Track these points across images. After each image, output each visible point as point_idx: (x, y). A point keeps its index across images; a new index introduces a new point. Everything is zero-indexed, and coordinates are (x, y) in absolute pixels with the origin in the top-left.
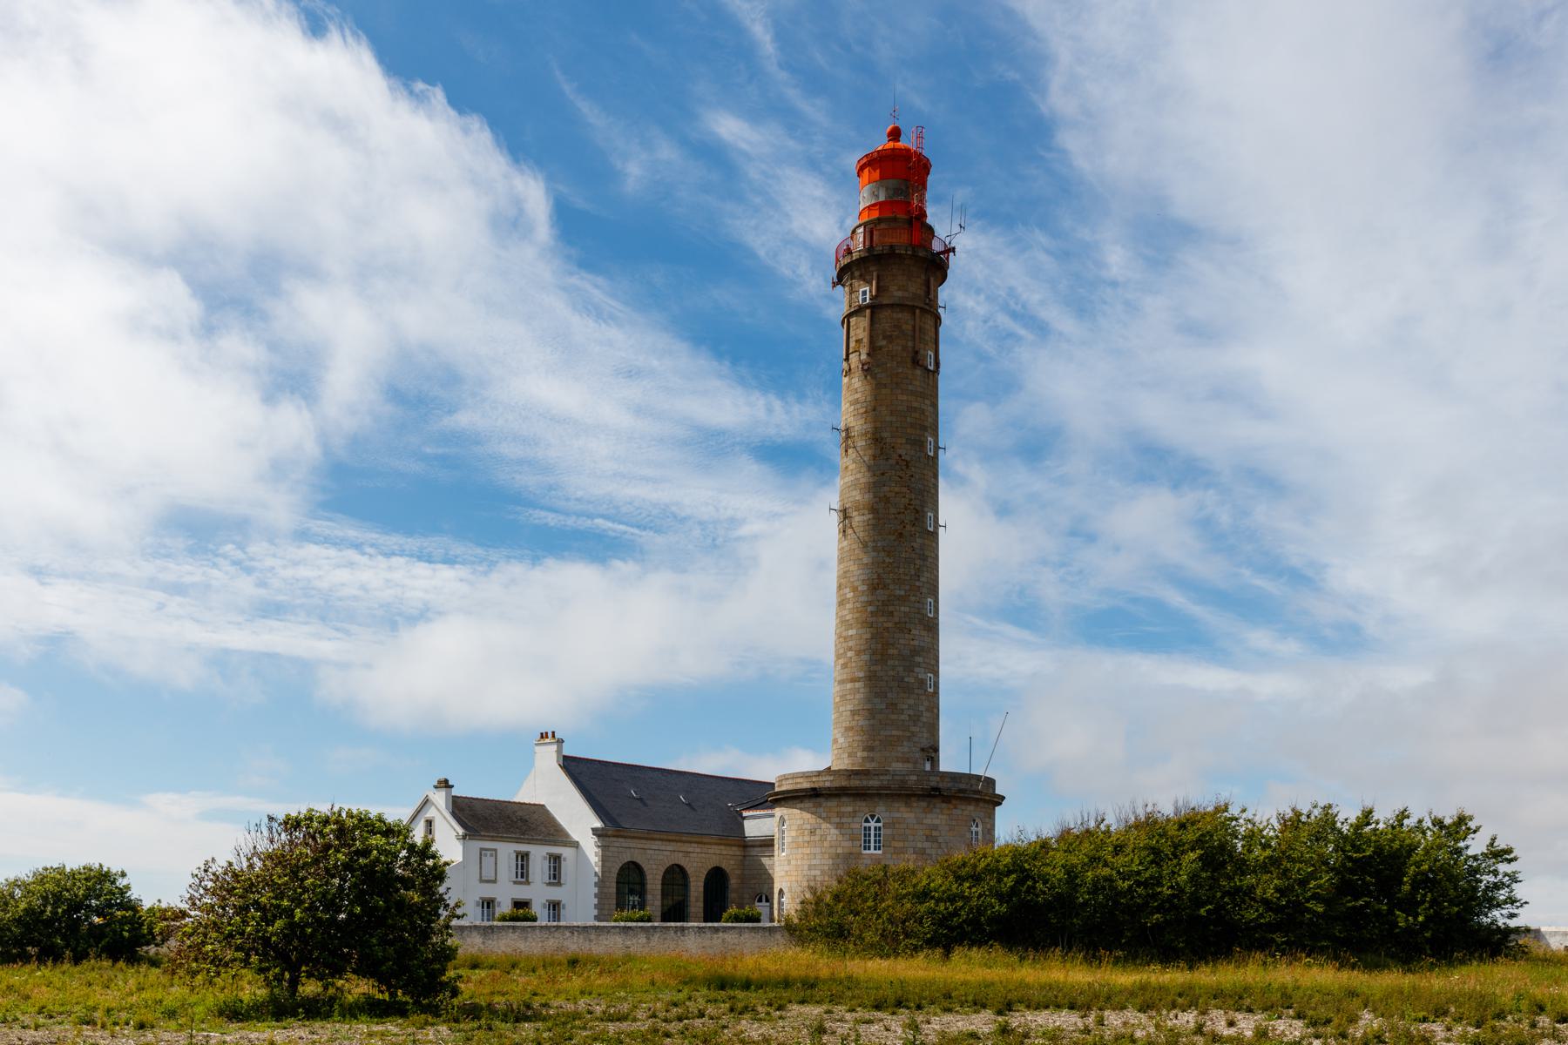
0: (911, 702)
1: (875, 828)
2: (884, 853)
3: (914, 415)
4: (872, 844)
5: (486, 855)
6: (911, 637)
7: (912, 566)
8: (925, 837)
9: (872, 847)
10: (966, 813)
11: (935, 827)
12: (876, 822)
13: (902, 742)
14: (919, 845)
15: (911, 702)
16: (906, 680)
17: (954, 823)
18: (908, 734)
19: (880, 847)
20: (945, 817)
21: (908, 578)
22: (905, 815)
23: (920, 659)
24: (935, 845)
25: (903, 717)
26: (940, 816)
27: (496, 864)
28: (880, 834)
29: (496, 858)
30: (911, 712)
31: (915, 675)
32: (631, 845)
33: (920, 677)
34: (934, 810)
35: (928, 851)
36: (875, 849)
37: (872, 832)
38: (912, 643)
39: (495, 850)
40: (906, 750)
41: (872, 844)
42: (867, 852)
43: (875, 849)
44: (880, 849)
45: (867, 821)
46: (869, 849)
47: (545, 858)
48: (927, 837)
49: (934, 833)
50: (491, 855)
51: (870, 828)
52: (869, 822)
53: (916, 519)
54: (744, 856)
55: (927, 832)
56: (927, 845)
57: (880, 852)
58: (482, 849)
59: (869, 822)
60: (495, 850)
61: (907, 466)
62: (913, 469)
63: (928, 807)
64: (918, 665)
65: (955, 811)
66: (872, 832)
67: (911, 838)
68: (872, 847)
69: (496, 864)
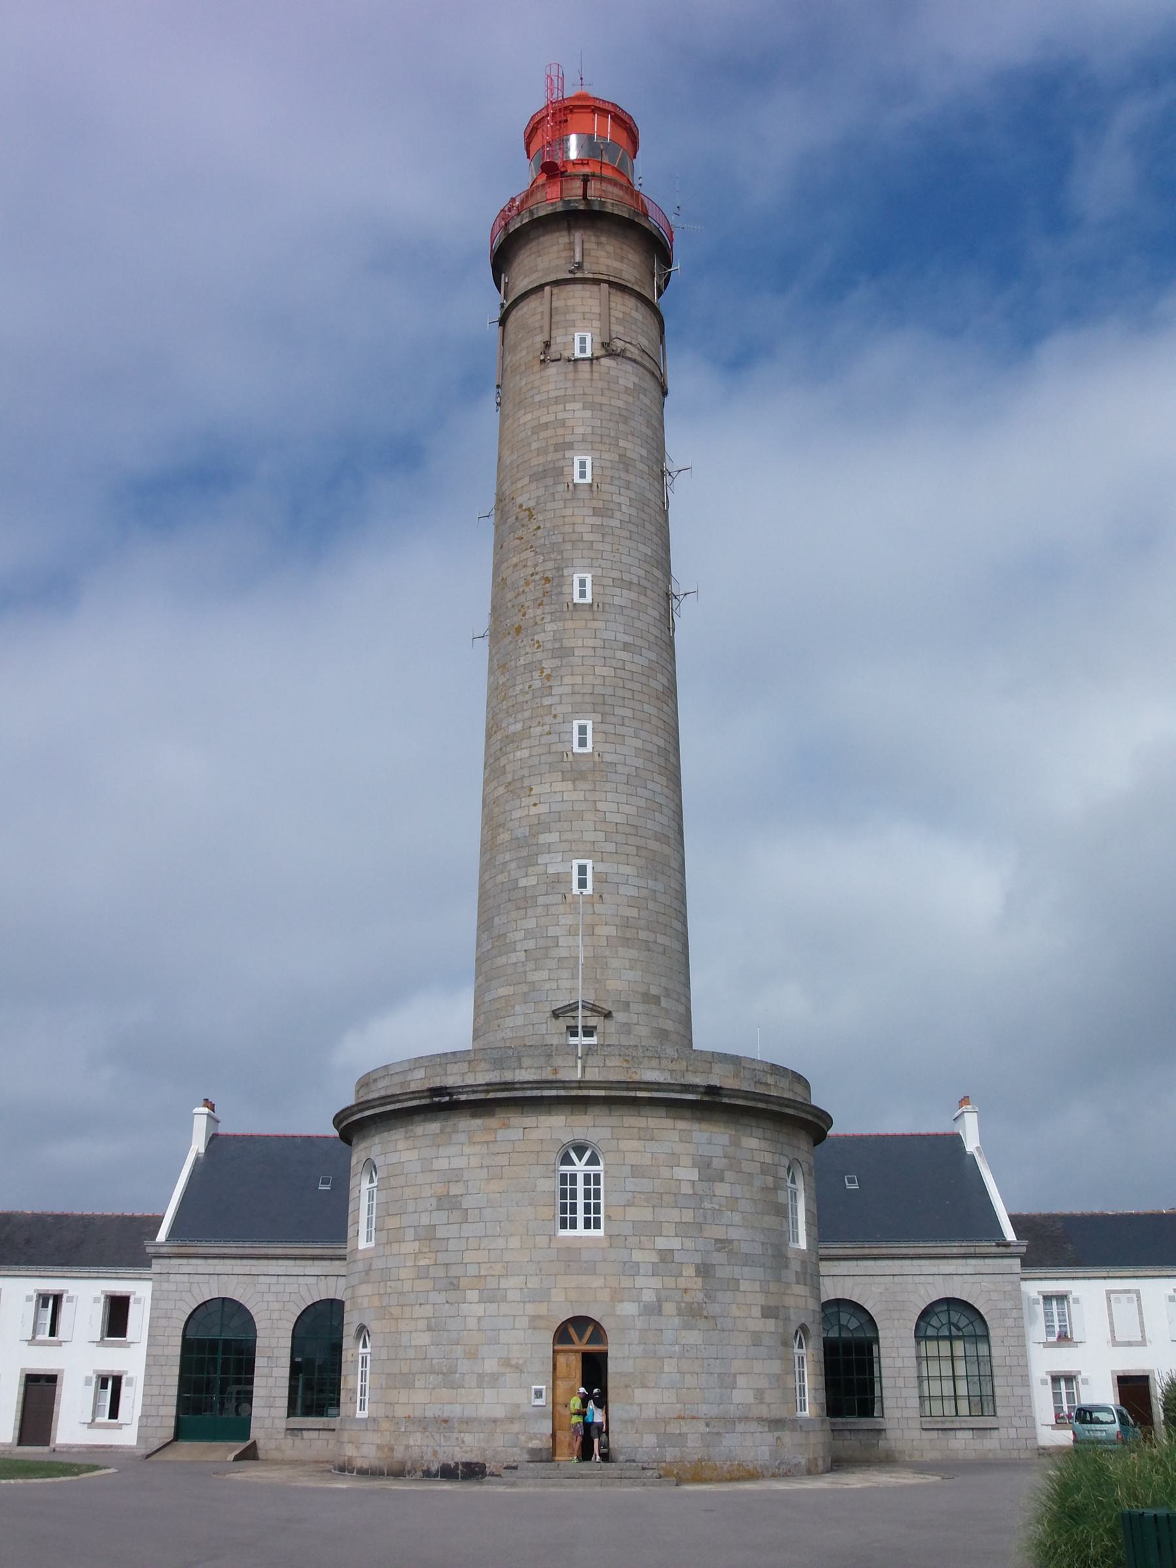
0: (531, 923)
1: (587, 1178)
2: (609, 1236)
3: (543, 435)
4: (580, 1215)
5: (1118, 1300)
6: (534, 800)
7: (536, 674)
8: (434, 1202)
9: (580, 1223)
10: (535, 1135)
11: (454, 1176)
12: (588, 1163)
13: (513, 1007)
14: (425, 1220)
15: (531, 923)
16: (523, 883)
17: (502, 1160)
18: (525, 988)
19: (597, 1220)
20: (477, 1149)
21: (528, 697)
22: (406, 1156)
23: (553, 837)
24: (456, 1216)
25: (513, 958)
26: (467, 1150)
27: (1141, 1313)
28: (597, 1192)
29: (1140, 1306)
30: (531, 944)
31: (539, 869)
32: (219, 1270)
33: (550, 870)
34: (455, 1137)
35: (441, 1232)
36: (587, 1225)
37: (580, 1187)
38: (534, 811)
39: (1137, 1292)
40: (520, 1021)
41: (580, 1215)
42: (568, 1232)
43: (587, 1225)
44: (597, 1226)
45: (567, 1161)
46: (574, 1226)
47: (88, 1382)
48: (439, 1198)
49: (455, 1190)
50: (1130, 1300)
51: (574, 1178)
52: (573, 1164)
53: (545, 593)
54: (354, 1298)
55: (440, 1189)
56: (440, 1217)
57: (600, 1233)
58: (1109, 1293)
59: (573, 1164)
60: (1137, 1292)
61: (531, 516)
62: (540, 517)
63: (442, 1131)
64: (549, 848)
65: (502, 1134)
66: (580, 1187)
67: (411, 1207)
68: (580, 1223)
69: (1141, 1313)
